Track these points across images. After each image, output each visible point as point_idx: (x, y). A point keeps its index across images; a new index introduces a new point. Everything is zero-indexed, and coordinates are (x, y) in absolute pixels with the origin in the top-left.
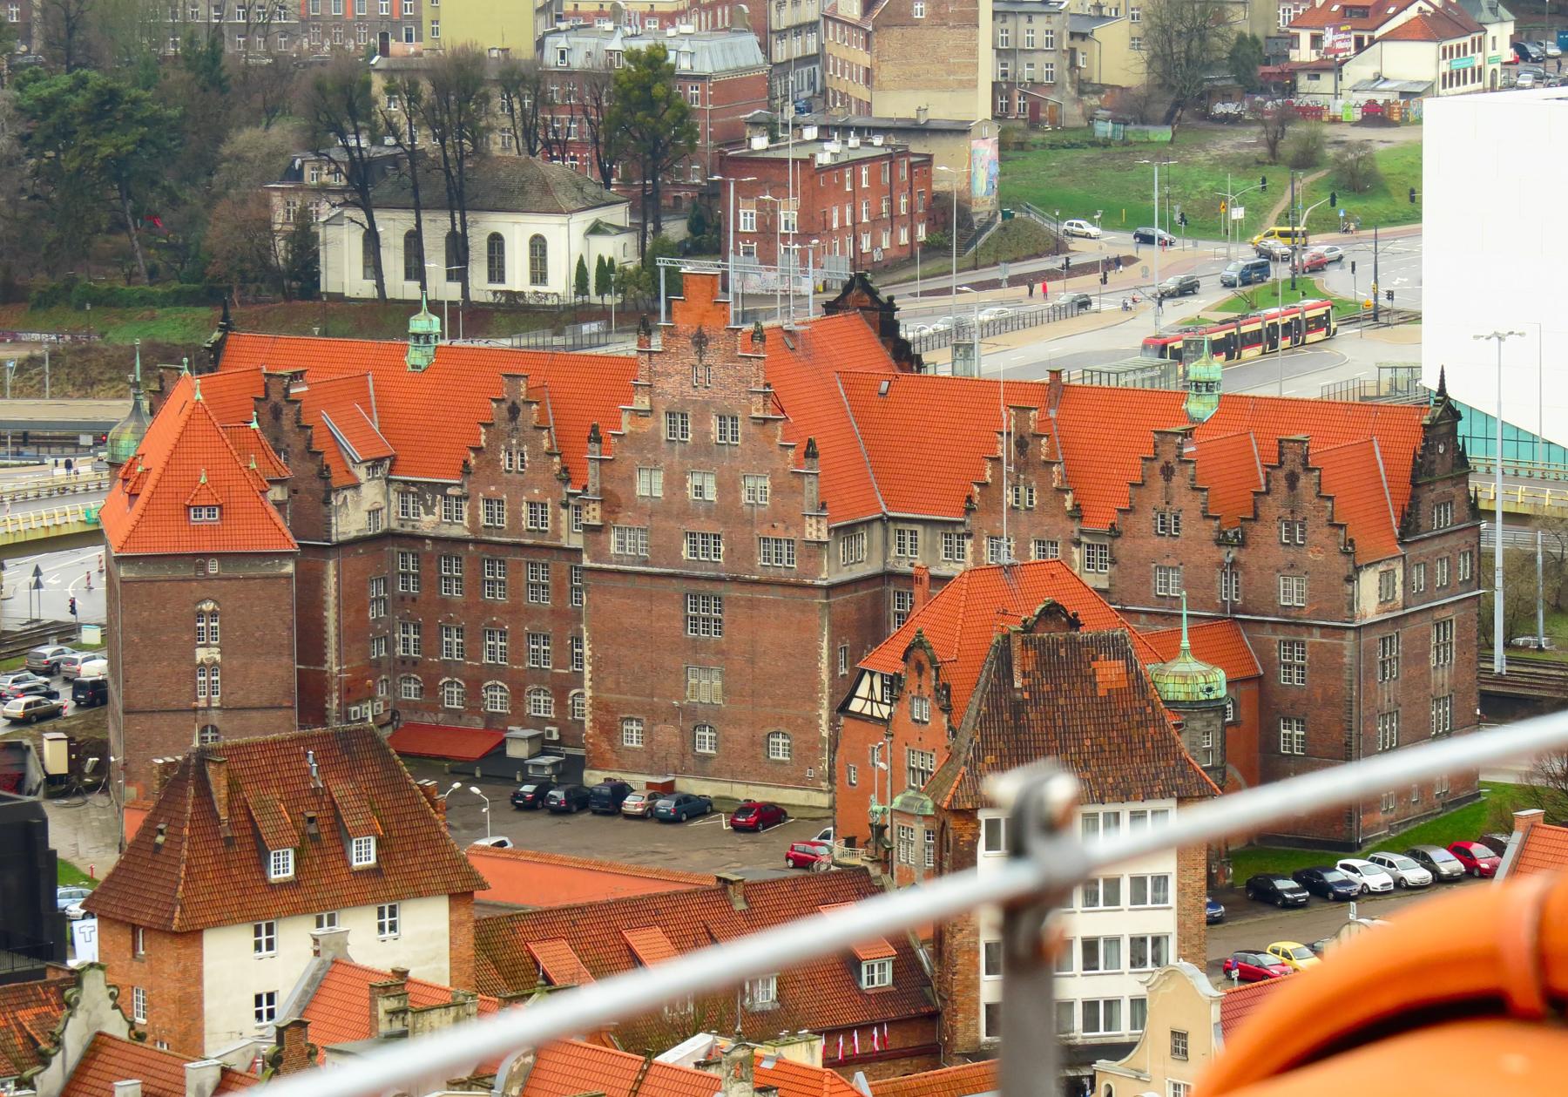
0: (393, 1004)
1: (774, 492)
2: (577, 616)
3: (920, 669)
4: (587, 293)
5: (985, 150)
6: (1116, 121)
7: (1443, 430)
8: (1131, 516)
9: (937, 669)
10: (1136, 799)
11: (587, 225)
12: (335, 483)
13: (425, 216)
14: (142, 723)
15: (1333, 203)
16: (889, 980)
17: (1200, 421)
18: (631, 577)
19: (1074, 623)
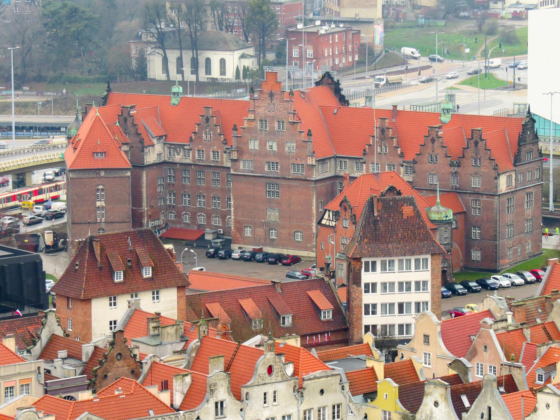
0: (154, 325)
1: (296, 148)
2: (229, 190)
3: (345, 209)
4: (240, 78)
5: (379, 29)
6: (426, 18)
7: (529, 126)
8: (420, 156)
9: (351, 209)
10: (417, 254)
11: (240, 55)
12: (145, 145)
13: (183, 52)
14: (78, 228)
15: (500, 47)
16: (331, 317)
17: (445, 123)
18: (247, 177)
19: (399, 193)
